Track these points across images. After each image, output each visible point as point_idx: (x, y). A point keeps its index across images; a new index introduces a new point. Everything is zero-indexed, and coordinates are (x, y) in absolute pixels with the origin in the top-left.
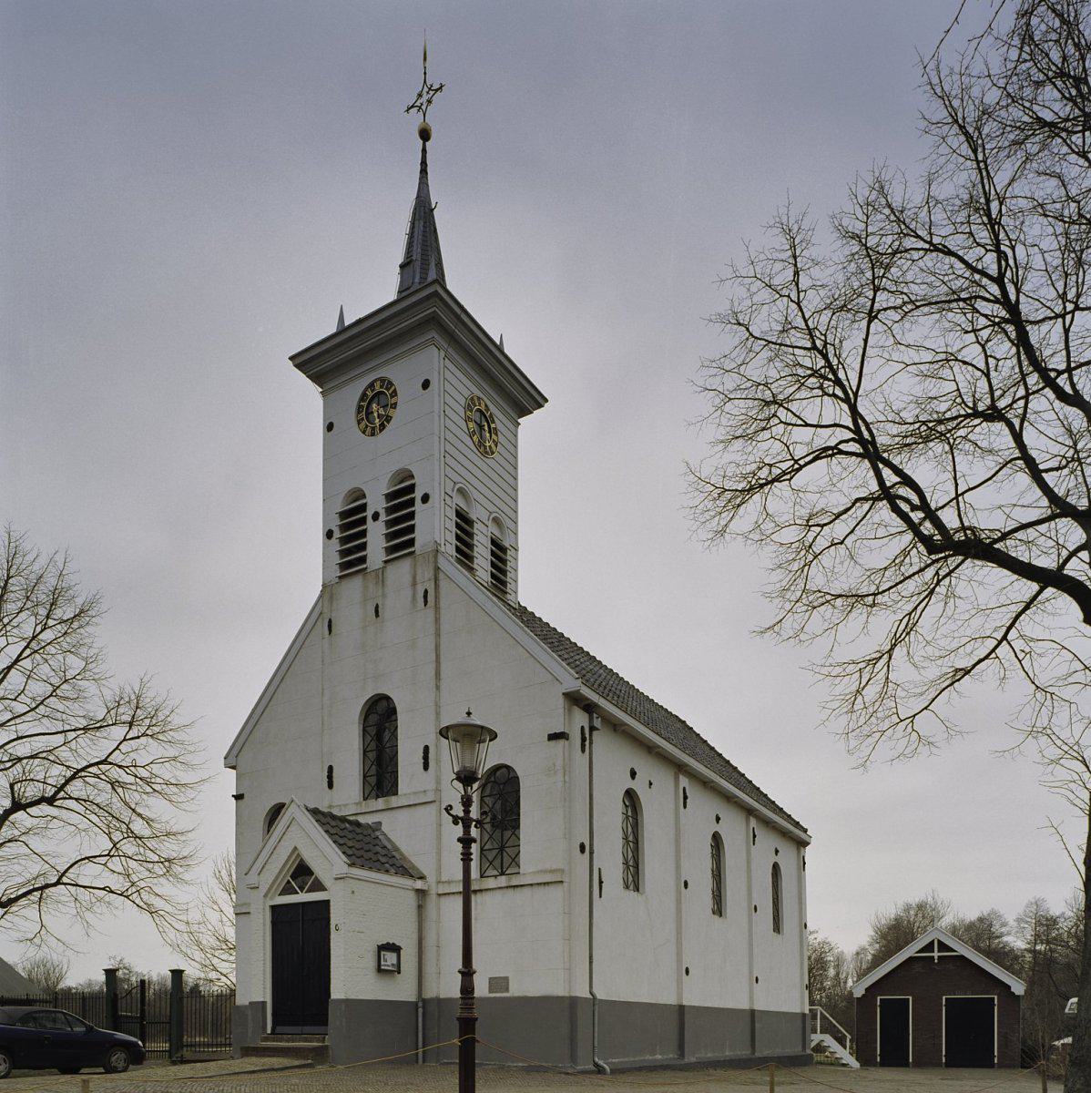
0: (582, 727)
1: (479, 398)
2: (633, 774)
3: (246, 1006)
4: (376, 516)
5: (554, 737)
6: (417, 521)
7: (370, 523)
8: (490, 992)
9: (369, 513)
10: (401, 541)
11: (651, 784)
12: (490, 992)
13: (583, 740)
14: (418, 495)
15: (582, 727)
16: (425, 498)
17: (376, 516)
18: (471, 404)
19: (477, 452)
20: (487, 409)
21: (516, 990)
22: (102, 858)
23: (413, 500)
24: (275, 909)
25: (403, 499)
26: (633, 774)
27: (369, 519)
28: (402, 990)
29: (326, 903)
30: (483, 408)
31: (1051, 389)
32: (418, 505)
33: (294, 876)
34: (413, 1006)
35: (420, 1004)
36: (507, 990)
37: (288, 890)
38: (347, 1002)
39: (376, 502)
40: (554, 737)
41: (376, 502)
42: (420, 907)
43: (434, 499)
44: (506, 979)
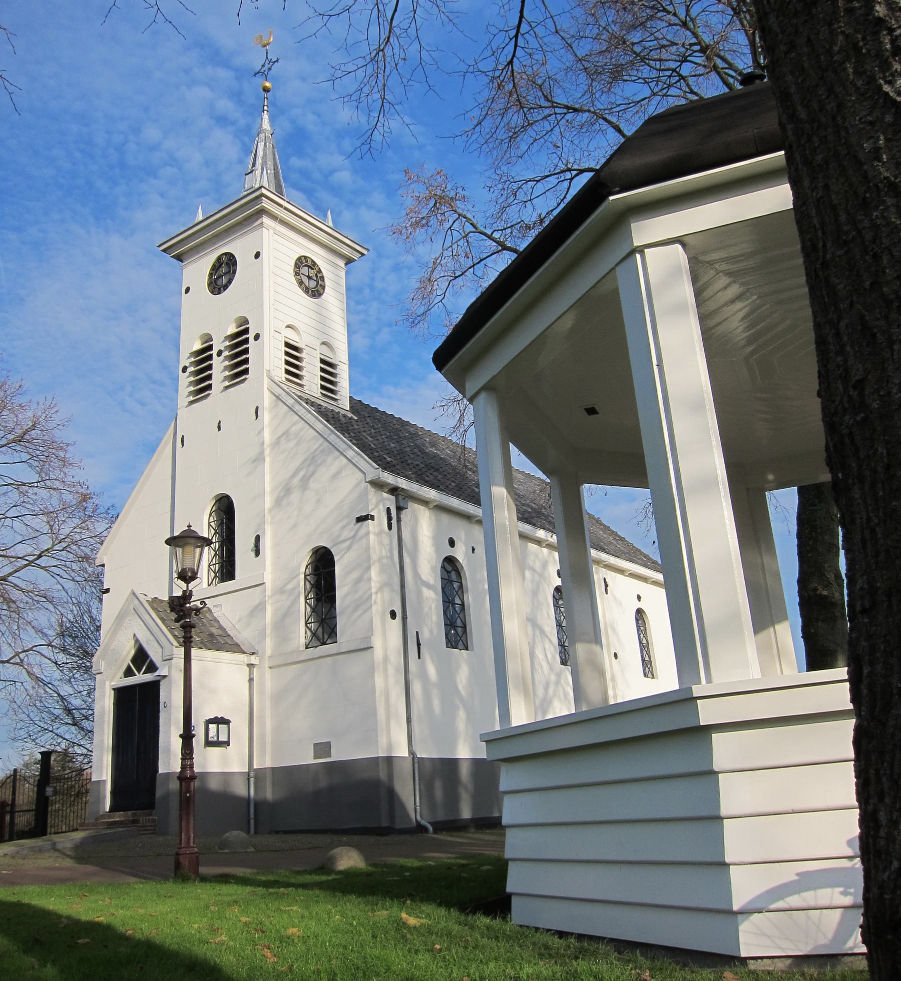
0: (388, 510)
2: (452, 543)
4: (220, 353)
9: (214, 352)
10: (239, 369)
11: (473, 550)
13: (390, 519)
14: (251, 336)
16: (257, 337)
21: (338, 755)
22: (43, 652)
23: (247, 339)
25: (240, 342)
26: (452, 543)
27: (251, 340)
31: (792, 189)
32: (252, 344)
33: (134, 660)
35: (252, 774)
41: (219, 344)
43: (265, 337)
44: (315, 745)
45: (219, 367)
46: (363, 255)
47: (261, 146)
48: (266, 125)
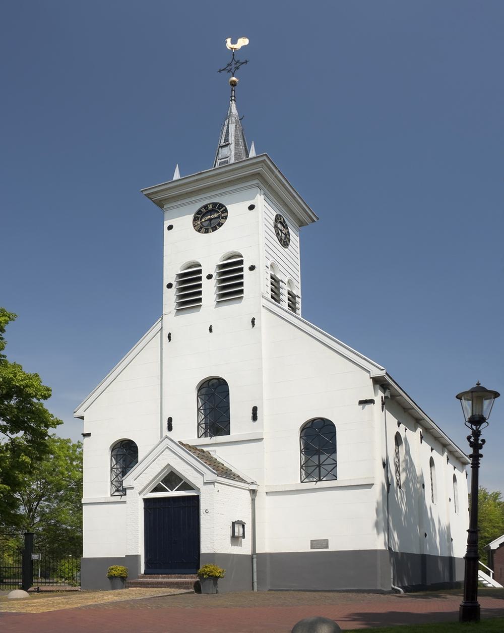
0: (382, 397)
1: (280, 216)
3: (461, 558)
5: (88, 435)
6: (202, 289)
7: (204, 281)
8: (311, 548)
12: (311, 548)
15: (382, 397)
17: (210, 277)
18: (278, 218)
19: (280, 244)
20: (285, 222)
21: (332, 548)
24: (146, 501)
28: (245, 549)
29: (196, 499)
30: (282, 220)
34: (251, 557)
35: (255, 556)
36: (327, 547)
37: (157, 489)
38: (204, 554)
39: (209, 267)
40: (363, 402)
42: (253, 500)
45: (209, 289)
46: (314, 221)
47: (232, 128)
48: (234, 110)
